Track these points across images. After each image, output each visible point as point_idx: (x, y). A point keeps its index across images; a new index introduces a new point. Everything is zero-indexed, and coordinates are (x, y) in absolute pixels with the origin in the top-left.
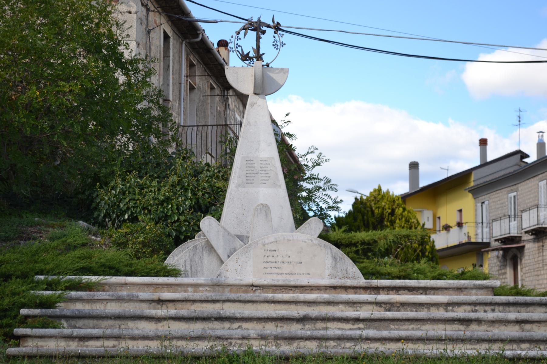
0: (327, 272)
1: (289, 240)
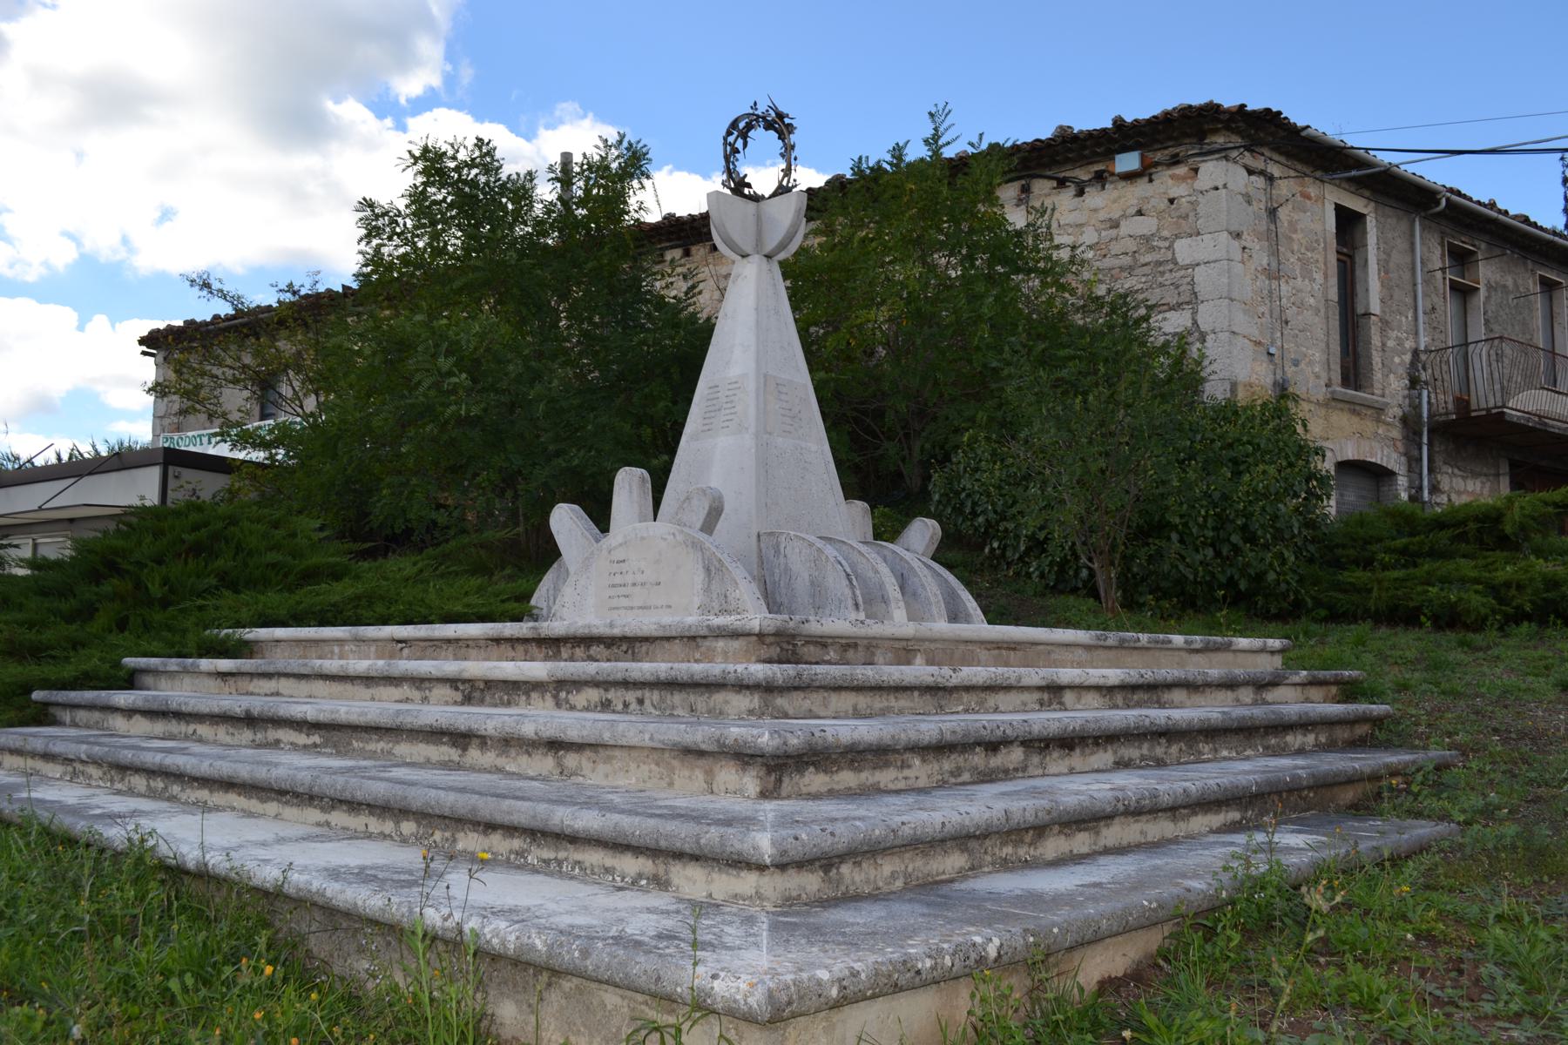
0: (697, 601)
1: (643, 538)
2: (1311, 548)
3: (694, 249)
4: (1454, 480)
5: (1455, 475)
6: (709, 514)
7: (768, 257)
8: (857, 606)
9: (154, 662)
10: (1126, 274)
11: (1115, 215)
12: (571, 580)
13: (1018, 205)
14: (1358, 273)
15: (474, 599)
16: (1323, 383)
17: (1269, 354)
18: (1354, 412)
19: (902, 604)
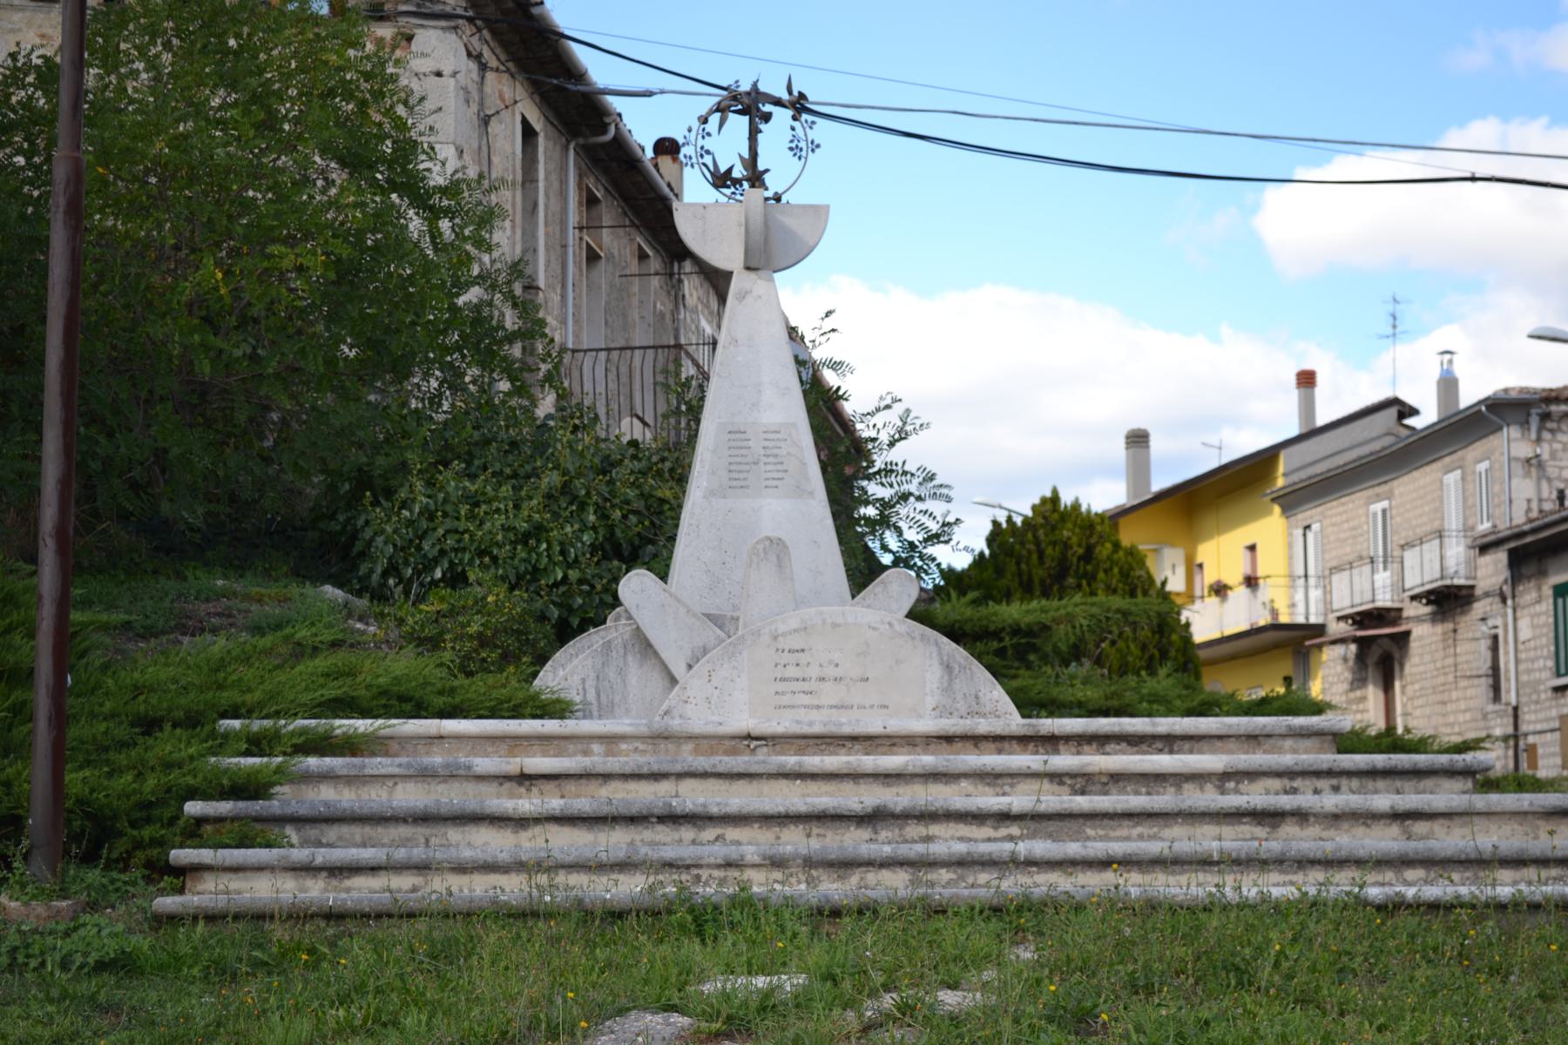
0: (930, 702)
1: (835, 625)
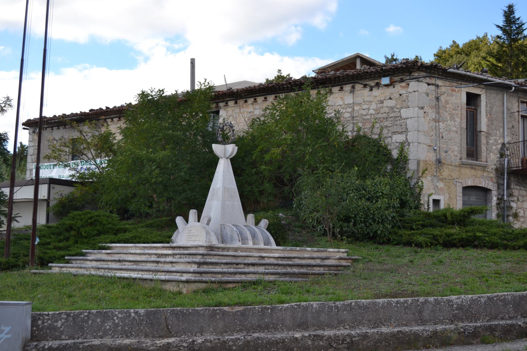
2: (399, 223)
3: (238, 101)
4: (521, 191)
5: (521, 190)
6: (208, 221)
7: (227, 158)
8: (239, 241)
9: (90, 251)
10: (385, 120)
11: (382, 99)
12: (180, 234)
13: (351, 93)
14: (478, 116)
15: (159, 238)
16: (458, 158)
17: (434, 149)
18: (472, 168)
19: (252, 240)
